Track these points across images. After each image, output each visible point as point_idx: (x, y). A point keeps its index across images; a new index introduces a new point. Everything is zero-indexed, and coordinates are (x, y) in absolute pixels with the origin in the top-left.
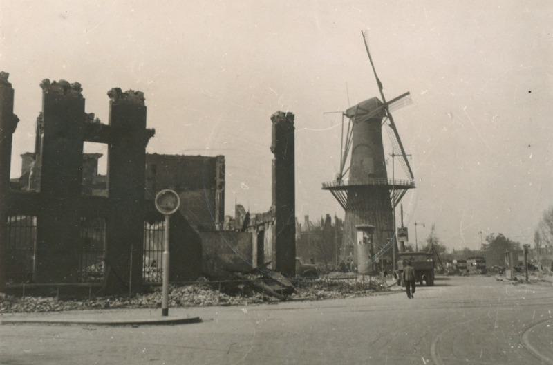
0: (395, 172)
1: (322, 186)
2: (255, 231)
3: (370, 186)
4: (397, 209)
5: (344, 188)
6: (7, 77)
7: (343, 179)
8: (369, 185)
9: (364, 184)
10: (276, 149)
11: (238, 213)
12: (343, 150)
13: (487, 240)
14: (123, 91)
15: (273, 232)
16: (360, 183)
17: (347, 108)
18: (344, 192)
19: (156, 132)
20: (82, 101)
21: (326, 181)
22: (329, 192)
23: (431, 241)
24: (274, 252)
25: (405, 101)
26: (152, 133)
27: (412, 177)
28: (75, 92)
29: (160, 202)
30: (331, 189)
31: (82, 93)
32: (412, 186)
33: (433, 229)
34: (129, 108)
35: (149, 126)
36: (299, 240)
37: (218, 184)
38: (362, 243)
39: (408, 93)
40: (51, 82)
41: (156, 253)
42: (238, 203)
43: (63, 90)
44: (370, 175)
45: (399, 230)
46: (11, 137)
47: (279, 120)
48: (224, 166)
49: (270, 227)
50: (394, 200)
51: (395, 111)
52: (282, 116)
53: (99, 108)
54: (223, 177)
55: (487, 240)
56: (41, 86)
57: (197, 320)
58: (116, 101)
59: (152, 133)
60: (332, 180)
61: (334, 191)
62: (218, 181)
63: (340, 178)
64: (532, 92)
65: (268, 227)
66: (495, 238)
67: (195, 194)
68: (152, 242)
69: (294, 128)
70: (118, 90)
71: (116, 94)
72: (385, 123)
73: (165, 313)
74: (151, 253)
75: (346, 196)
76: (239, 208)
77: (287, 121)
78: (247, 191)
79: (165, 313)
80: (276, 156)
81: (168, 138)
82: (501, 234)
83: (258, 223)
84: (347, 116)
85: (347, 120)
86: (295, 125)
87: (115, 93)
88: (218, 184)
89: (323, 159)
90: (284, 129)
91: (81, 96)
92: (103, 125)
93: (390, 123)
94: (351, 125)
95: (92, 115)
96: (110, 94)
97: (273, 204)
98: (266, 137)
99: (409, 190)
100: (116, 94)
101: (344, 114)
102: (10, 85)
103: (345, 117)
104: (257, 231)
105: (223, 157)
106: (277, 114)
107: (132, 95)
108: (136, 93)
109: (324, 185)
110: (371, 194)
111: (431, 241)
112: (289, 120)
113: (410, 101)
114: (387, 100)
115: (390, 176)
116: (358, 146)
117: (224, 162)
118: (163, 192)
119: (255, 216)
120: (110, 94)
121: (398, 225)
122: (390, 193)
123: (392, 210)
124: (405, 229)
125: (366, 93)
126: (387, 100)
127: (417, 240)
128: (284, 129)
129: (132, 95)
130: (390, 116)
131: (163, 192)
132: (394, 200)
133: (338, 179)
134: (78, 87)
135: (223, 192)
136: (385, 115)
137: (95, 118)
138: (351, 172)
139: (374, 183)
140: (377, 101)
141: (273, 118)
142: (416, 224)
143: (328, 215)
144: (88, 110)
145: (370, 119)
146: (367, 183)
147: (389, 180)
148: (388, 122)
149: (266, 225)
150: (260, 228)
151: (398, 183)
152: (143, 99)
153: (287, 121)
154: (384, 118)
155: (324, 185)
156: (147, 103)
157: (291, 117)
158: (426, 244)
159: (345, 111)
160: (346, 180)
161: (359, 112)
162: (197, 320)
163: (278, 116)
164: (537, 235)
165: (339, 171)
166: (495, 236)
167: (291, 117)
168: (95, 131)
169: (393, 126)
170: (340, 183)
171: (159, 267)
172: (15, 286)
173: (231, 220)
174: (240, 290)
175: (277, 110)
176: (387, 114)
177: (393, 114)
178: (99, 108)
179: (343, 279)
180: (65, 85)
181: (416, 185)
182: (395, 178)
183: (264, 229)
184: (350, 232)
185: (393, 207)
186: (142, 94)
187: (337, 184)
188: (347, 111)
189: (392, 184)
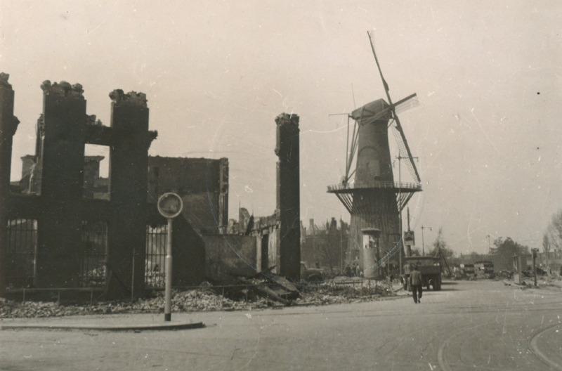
0: (402, 175)
1: (327, 189)
2: (260, 235)
3: (376, 189)
4: (404, 213)
5: (349, 191)
6: (7, 79)
7: (348, 182)
8: (375, 188)
9: (370, 187)
10: (280, 151)
11: (241, 216)
12: (349, 153)
13: (495, 244)
14: (125, 93)
15: (277, 236)
16: (366, 186)
17: (353, 110)
18: (350, 195)
19: (159, 134)
20: (83, 103)
21: (331, 184)
22: (334, 195)
23: (438, 244)
24: (279, 256)
25: (411, 103)
26: (154, 135)
27: (419, 180)
28: (77, 93)
29: (162, 205)
30: (337, 192)
31: (84, 94)
32: (418, 189)
33: (440, 232)
34: (131, 110)
35: (151, 128)
36: (303, 243)
37: (221, 187)
38: (368, 247)
39: (414, 95)
40: (52, 83)
41: (158, 257)
42: (242, 206)
43: (64, 92)
44: (376, 178)
45: (406, 233)
46: (12, 139)
47: (283, 122)
48: (227, 169)
49: (274, 230)
50: (401, 204)
51: (401, 113)
52: (286, 118)
53: (100, 110)
54: (226, 179)
55: (495, 244)
56: (42, 87)
57: (200, 326)
58: (118, 102)
59: (154, 135)
60: (337, 183)
61: (340, 195)
62: (222, 184)
63: (345, 181)
64: (541, 93)
65: (272, 231)
66: (503, 242)
67: (198, 197)
68: (154, 246)
69: (299, 130)
70: (120, 92)
71: (118, 96)
72: (392, 125)
73: (168, 318)
74: (154, 257)
75: (352, 199)
76: (243, 211)
77: (292, 123)
78: (251, 194)
79: (168, 318)
80: (280, 159)
81: (171, 140)
82: (509, 238)
83: (262, 226)
84: (353, 118)
85: (353, 122)
86: (299, 127)
87: (117, 94)
88: (221, 187)
89: (328, 161)
90: (288, 131)
91: (83, 97)
92: (105, 127)
93: (396, 125)
94: (357, 127)
95: (94, 117)
96: (112, 96)
97: (277, 207)
98: (270, 139)
99: (416, 194)
100: (118, 96)
101: (349, 116)
102: (10, 86)
103: (351, 119)
104: (261, 235)
105: (226, 160)
106: (282, 116)
107: (134, 97)
108: (139, 95)
109: (329, 188)
110: (377, 197)
111: (438, 244)
112: (294, 122)
113: (417, 103)
114: (393, 102)
115: (396, 179)
116: (364, 148)
117: (227, 165)
118: (166, 195)
119: (259, 220)
120: (112, 96)
121: (405, 229)
122: (396, 197)
123: (398, 213)
124: (412, 233)
125: (372, 94)
126: (393, 102)
127: (424, 244)
128: (288, 131)
129: (134, 97)
130: (396, 118)
131: (166, 195)
132: (401, 204)
133: (343, 182)
134: (79, 89)
135: (227, 195)
136: (391, 117)
137: (97, 120)
138: (357, 175)
139: (380, 186)
140: (383, 103)
141: (277, 120)
142: (422, 228)
143: (333, 219)
144: (89, 112)
145: (376, 121)
146: (373, 186)
147: (395, 183)
148: (395, 124)
149: (270, 228)
150: (265, 232)
151: (404, 186)
152: (146, 101)
153: (292, 123)
154: (391, 120)
155: (329, 188)
156: (149, 105)
157: (295, 119)
158: (433, 248)
159: (350, 112)
160: (352, 183)
161: (365, 113)
162: (200, 326)
163: (282, 118)
164: (546, 239)
165: (344, 174)
166: (504, 240)
167: (295, 119)
168: (97, 133)
169: (399, 128)
170: (345, 186)
171: (162, 271)
172: (15, 290)
173: (235, 223)
174: (244, 294)
175: (282, 112)
176: (393, 116)
177: (399, 116)
178: (100, 110)
179: (348, 283)
180: (66, 87)
181: (422, 189)
182: (402, 181)
183: (269, 232)
184: (356, 236)
185: (399, 210)
186: (144, 95)
187: (342, 187)
188: (353, 112)
189: (399, 187)
